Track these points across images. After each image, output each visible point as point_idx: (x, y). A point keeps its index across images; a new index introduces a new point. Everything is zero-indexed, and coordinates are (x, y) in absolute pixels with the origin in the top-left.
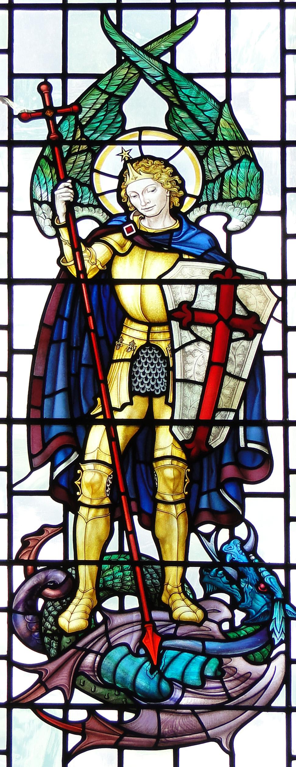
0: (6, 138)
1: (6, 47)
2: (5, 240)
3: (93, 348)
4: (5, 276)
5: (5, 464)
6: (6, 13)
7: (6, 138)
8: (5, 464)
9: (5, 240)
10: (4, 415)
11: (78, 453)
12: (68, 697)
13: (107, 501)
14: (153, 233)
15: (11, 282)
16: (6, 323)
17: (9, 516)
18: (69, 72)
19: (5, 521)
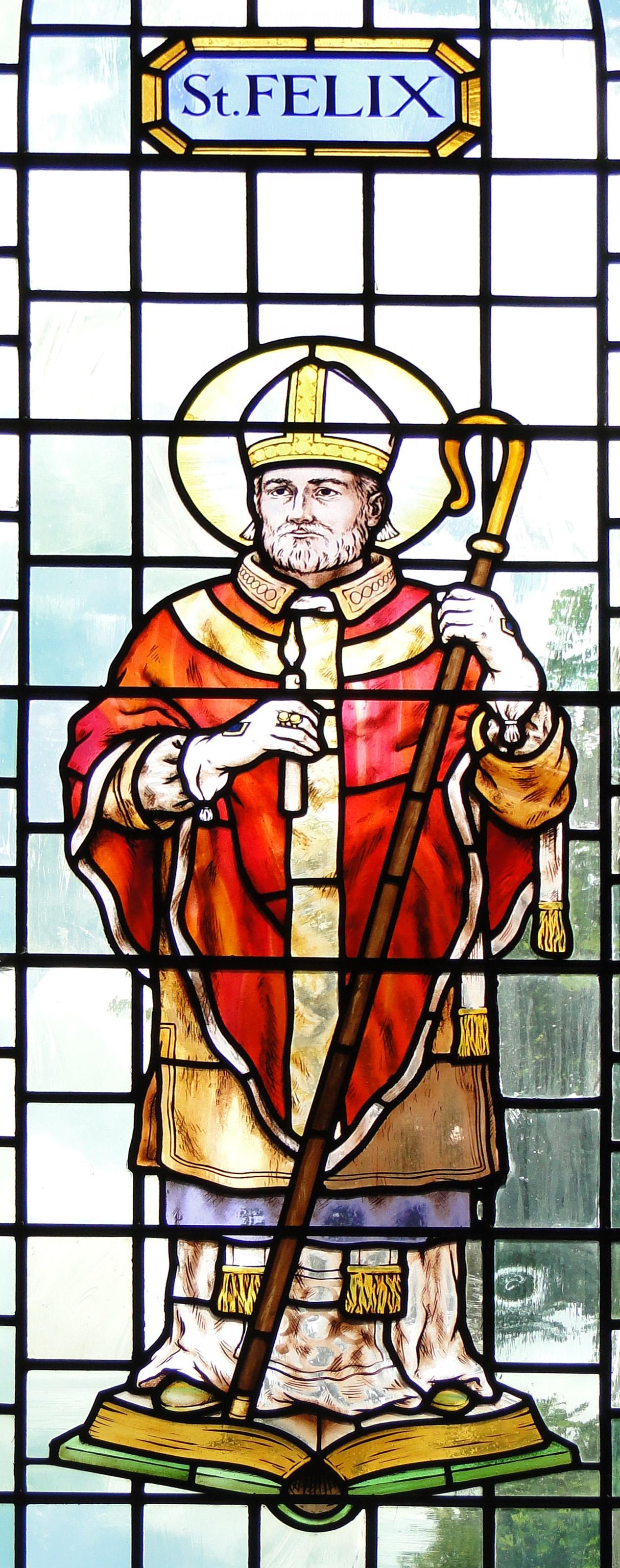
0: (12, 949)
1: (16, 61)
2: (12, 352)
3: (169, 1461)
4: (14, 413)
5: (10, 1041)
6: (13, 440)
7: (12, 949)
8: (11, 1311)
9: (12, 352)
10: (9, 1486)
11: (314, 152)
12: (466, 965)
13: (485, 1010)
14: (426, 1185)
15: (21, 961)
16: (13, 242)
17: (18, 1409)
18: (145, 24)
19: (11, 1152)
